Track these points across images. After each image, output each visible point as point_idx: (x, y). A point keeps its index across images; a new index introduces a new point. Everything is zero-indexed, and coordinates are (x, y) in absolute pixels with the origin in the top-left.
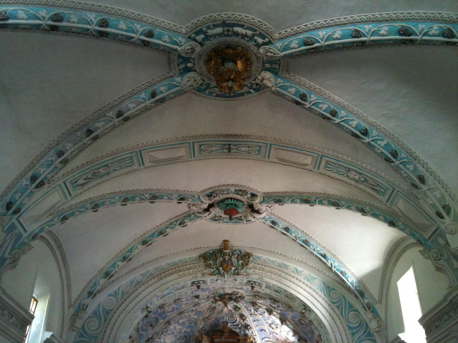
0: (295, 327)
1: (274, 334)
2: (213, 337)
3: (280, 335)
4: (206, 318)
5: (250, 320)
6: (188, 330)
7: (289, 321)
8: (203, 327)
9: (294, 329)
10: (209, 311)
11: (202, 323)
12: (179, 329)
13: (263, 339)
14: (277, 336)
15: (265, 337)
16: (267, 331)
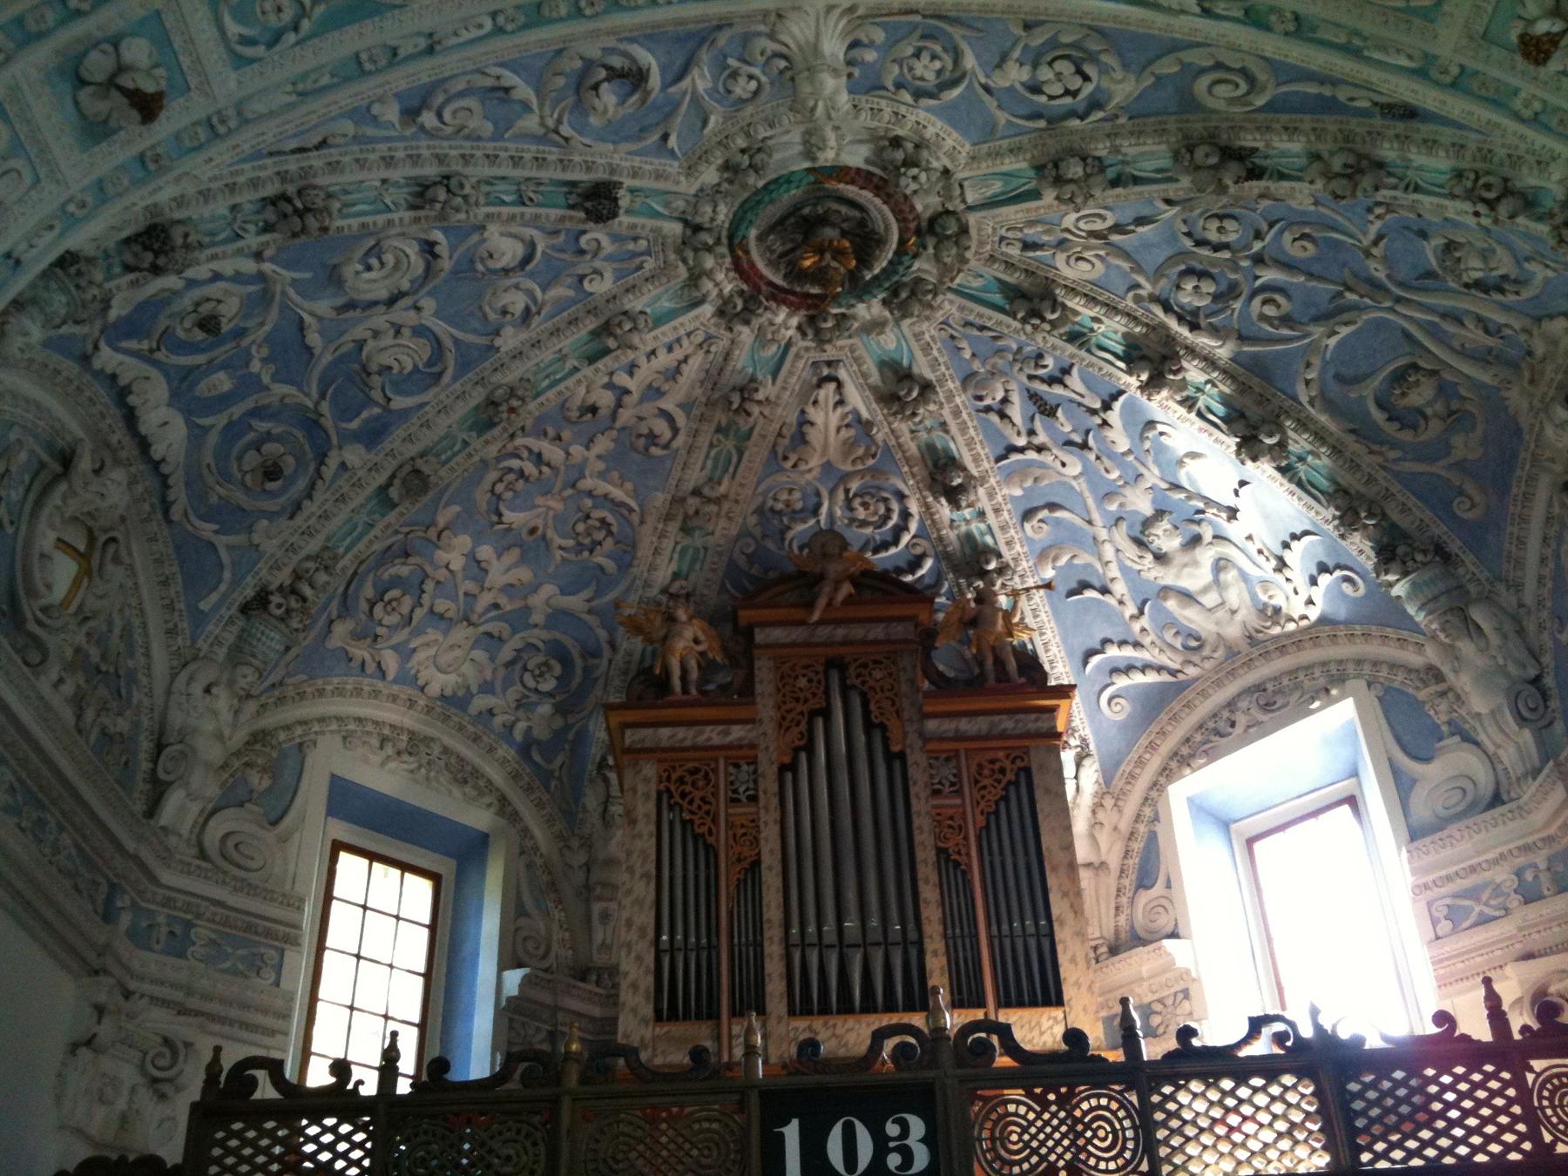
0: (1354, 466)
1: (1171, 604)
2: (745, 615)
3: (1210, 599)
4: (696, 492)
5: (993, 511)
6: (576, 602)
7: (1304, 424)
8: (676, 576)
9: (1346, 479)
10: (708, 430)
11: (668, 544)
12: (508, 588)
13: (1090, 653)
14: (1191, 617)
15: (1106, 641)
16: (1120, 588)
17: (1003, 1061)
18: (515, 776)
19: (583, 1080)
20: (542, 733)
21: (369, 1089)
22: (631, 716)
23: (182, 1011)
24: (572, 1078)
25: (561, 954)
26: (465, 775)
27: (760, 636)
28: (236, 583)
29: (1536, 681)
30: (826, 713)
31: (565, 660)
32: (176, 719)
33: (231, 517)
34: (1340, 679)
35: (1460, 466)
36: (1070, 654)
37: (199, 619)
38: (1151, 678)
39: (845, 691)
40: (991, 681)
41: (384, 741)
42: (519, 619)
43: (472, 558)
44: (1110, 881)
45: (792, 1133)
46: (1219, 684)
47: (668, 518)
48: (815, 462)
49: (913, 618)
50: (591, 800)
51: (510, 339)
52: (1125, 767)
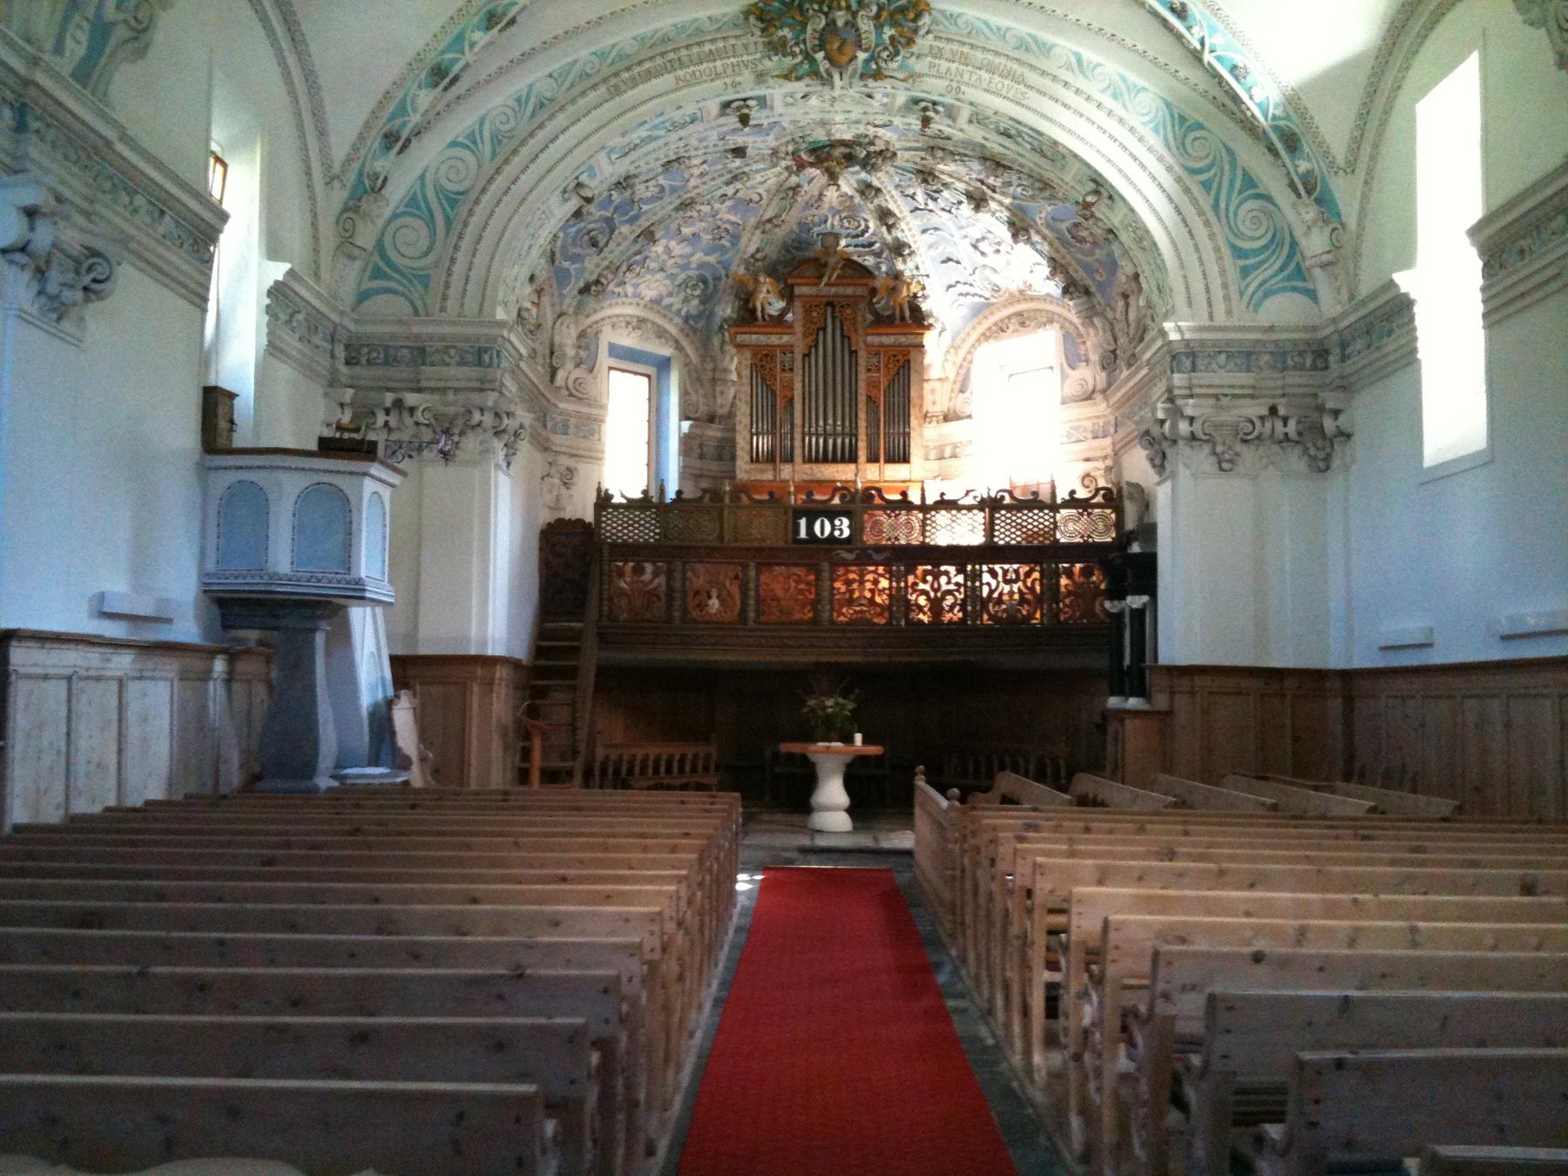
5: (908, 229)
7: (1038, 232)
8: (758, 250)
17: (877, 501)
18: (682, 330)
24: (727, 500)
25: (703, 409)
26: (661, 334)
27: (797, 291)
29: (1113, 352)
30: (824, 329)
31: (705, 282)
32: (557, 339)
33: (576, 258)
34: (1051, 321)
37: (562, 297)
38: (977, 299)
39: (834, 318)
40: (898, 321)
41: (628, 323)
42: (684, 267)
43: (667, 247)
44: (948, 386)
45: (803, 522)
47: (756, 228)
50: (716, 341)
51: (693, 183)
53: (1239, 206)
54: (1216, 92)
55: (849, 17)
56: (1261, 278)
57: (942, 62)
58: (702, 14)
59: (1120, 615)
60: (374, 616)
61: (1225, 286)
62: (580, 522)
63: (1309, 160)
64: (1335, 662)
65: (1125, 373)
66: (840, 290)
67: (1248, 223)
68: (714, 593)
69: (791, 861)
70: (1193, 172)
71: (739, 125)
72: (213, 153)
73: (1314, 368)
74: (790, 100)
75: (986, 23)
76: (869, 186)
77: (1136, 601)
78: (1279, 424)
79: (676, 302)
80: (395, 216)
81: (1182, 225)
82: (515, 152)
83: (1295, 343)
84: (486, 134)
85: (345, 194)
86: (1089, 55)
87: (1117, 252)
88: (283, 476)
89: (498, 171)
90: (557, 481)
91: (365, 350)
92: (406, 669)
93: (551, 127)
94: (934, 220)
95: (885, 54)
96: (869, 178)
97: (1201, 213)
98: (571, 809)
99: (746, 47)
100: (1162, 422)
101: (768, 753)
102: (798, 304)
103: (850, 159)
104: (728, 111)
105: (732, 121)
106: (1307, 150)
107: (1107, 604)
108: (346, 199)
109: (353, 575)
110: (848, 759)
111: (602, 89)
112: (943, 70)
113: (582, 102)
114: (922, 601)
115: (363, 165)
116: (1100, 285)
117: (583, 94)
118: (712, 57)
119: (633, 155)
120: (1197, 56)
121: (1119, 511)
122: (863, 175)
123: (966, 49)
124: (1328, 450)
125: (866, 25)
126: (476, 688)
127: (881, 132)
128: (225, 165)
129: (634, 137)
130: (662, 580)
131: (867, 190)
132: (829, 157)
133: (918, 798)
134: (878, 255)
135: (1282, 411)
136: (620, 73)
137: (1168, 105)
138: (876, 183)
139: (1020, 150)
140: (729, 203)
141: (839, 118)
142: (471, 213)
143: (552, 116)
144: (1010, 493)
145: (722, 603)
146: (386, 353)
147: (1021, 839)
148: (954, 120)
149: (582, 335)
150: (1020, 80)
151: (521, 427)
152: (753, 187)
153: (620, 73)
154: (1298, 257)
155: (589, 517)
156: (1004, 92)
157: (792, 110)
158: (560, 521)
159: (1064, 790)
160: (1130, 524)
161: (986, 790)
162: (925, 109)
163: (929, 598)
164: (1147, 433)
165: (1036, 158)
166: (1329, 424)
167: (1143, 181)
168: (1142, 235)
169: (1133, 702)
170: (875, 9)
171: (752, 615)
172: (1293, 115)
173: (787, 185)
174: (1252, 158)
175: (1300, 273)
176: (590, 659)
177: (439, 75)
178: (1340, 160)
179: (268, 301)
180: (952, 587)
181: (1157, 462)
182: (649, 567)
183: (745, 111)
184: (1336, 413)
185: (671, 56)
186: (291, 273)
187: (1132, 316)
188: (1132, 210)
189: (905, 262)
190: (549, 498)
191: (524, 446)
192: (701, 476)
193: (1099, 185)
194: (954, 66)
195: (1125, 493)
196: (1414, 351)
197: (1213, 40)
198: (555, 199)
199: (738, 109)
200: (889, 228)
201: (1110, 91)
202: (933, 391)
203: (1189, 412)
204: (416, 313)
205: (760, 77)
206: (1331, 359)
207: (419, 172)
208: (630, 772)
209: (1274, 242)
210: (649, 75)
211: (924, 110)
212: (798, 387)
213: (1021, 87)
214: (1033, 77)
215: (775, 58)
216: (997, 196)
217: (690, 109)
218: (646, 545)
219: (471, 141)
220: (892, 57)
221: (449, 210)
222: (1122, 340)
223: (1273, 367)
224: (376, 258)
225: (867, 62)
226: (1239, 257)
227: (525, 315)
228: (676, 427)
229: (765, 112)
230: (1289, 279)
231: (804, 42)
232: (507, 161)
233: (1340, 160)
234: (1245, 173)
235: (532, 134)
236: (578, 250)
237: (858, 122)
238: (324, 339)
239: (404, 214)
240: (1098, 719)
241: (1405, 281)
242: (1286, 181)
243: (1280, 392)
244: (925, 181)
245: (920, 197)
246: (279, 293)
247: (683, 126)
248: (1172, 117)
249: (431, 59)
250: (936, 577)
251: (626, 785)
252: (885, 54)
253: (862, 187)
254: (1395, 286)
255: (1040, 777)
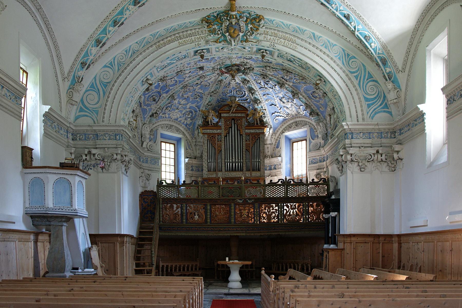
1: (285, 108)
5: (259, 94)
6: (194, 105)
7: (301, 95)
16: (277, 105)
19: (201, 184)
20: (189, 123)
21: (177, 184)
22: (204, 128)
23: (149, 170)
24: (200, 184)
27: (222, 115)
28: (149, 113)
29: (326, 134)
30: (231, 128)
32: (143, 132)
33: (148, 105)
35: (321, 104)
36: (270, 113)
37: (144, 118)
39: (234, 124)
41: (167, 127)
46: (291, 120)
48: (231, 87)
49: (245, 113)
50: (196, 132)
51: (187, 79)
52: (277, 130)
53: (367, 83)
54: (359, 45)
55: (237, 21)
56: (374, 108)
57: (268, 36)
58: (187, 21)
59: (328, 219)
60: (83, 221)
61: (362, 111)
62: (152, 191)
63: (390, 68)
64: (396, 232)
65: (330, 141)
66: (237, 115)
67: (370, 89)
68: (196, 214)
69: (222, 298)
70: (352, 73)
71: (201, 59)
72: (21, 68)
73: (391, 138)
74: (218, 50)
75: (282, 23)
76: (245, 80)
77: (333, 214)
78: (379, 156)
79: (183, 119)
80: (87, 91)
81: (346, 87)
82: (126, 68)
83: (385, 129)
84: (116, 63)
85: (69, 83)
86: (317, 33)
87: (327, 100)
88: (49, 175)
89: (120, 75)
90: (145, 179)
91: (78, 135)
92: (95, 238)
93: (138, 60)
94: (267, 91)
95: (249, 34)
96: (245, 77)
97: (354, 86)
98: (145, 283)
99: (202, 32)
100: (342, 155)
101: (216, 264)
102: (223, 119)
103: (239, 70)
104: (197, 54)
105: (198, 57)
106: (389, 64)
107: (324, 215)
108: (67, 83)
109: (74, 208)
110: (241, 266)
111: (154, 46)
112: (268, 39)
113: (147, 51)
114: (264, 215)
115: (75, 73)
116: (322, 113)
117: (148, 48)
118: (190, 35)
119: (165, 69)
120: (353, 33)
121: (328, 186)
122: (243, 76)
123: (276, 32)
124: (395, 164)
125: (242, 24)
126: (118, 244)
127: (248, 61)
128: (27, 73)
129: (165, 63)
130: (179, 210)
131: (245, 81)
132: (232, 70)
133: (262, 278)
134: (249, 103)
135: (380, 152)
136: (160, 41)
137: (344, 50)
138: (248, 79)
139: (295, 66)
140: (199, 86)
141: (234, 56)
142: (111, 89)
143: (137, 57)
144: (293, 180)
145: (199, 217)
146: (85, 137)
147: (292, 291)
148: (273, 56)
149: (151, 130)
150: (294, 42)
151: (131, 160)
152: (206, 81)
153: (160, 41)
154: (386, 101)
155: (155, 190)
156: (289, 46)
157: (218, 53)
158: (146, 191)
159: (309, 274)
160: (331, 190)
161: (284, 275)
162: (263, 52)
163: (266, 214)
164: (337, 159)
165: (300, 68)
166: (396, 156)
167: (336, 77)
168: (335, 94)
169: (332, 246)
170: (245, 18)
171: (209, 221)
172: (385, 53)
173: (218, 80)
174: (371, 68)
175: (386, 106)
176: (156, 236)
177: (98, 42)
178: (400, 68)
179: (44, 118)
180: (274, 211)
181: (340, 169)
182: (175, 206)
183: (203, 54)
184: (398, 152)
185: (177, 35)
186: (50, 109)
187: (332, 122)
188: (332, 85)
189: (258, 105)
190: (142, 184)
191: (132, 166)
192: (192, 176)
193: (321, 77)
194: (272, 37)
195: (330, 180)
196: (424, 130)
197: (359, 27)
198: (139, 85)
199: (200, 53)
200: (252, 94)
201: (324, 46)
202: (268, 148)
203: (351, 152)
204: (95, 123)
205: (207, 42)
206: (396, 134)
207: (93, 76)
208: (171, 270)
209: (378, 96)
210: (170, 42)
211: (262, 52)
212: (223, 146)
213: (295, 44)
214: (298, 41)
215: (212, 35)
216: (288, 83)
217: (184, 53)
218: (174, 199)
219: (111, 64)
220: (251, 35)
221: (104, 88)
222: (329, 130)
223: (378, 137)
224: (81, 105)
225: (243, 36)
226: (367, 101)
227: (131, 123)
228: (183, 160)
229: (210, 54)
230: (383, 108)
231: (222, 29)
232: (123, 72)
233: (400, 68)
234: (369, 73)
235: (131, 62)
236: (149, 103)
237: (241, 57)
238: (64, 132)
239: (90, 90)
240: (321, 252)
241: (421, 107)
242: (382, 75)
243: (380, 145)
244: (264, 78)
245: (262, 84)
246: (46, 115)
247: (182, 59)
248: (345, 54)
249: (95, 37)
250: (269, 208)
251: (172, 275)
252: (249, 34)
253: (243, 80)
254: (419, 109)
255: (302, 270)
